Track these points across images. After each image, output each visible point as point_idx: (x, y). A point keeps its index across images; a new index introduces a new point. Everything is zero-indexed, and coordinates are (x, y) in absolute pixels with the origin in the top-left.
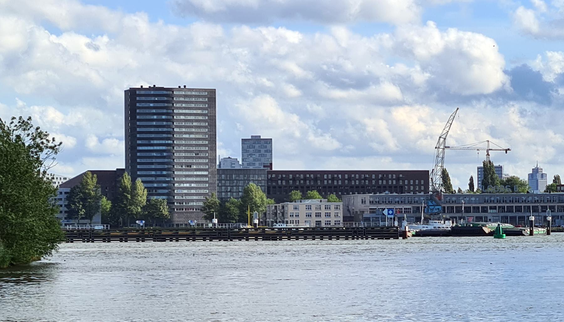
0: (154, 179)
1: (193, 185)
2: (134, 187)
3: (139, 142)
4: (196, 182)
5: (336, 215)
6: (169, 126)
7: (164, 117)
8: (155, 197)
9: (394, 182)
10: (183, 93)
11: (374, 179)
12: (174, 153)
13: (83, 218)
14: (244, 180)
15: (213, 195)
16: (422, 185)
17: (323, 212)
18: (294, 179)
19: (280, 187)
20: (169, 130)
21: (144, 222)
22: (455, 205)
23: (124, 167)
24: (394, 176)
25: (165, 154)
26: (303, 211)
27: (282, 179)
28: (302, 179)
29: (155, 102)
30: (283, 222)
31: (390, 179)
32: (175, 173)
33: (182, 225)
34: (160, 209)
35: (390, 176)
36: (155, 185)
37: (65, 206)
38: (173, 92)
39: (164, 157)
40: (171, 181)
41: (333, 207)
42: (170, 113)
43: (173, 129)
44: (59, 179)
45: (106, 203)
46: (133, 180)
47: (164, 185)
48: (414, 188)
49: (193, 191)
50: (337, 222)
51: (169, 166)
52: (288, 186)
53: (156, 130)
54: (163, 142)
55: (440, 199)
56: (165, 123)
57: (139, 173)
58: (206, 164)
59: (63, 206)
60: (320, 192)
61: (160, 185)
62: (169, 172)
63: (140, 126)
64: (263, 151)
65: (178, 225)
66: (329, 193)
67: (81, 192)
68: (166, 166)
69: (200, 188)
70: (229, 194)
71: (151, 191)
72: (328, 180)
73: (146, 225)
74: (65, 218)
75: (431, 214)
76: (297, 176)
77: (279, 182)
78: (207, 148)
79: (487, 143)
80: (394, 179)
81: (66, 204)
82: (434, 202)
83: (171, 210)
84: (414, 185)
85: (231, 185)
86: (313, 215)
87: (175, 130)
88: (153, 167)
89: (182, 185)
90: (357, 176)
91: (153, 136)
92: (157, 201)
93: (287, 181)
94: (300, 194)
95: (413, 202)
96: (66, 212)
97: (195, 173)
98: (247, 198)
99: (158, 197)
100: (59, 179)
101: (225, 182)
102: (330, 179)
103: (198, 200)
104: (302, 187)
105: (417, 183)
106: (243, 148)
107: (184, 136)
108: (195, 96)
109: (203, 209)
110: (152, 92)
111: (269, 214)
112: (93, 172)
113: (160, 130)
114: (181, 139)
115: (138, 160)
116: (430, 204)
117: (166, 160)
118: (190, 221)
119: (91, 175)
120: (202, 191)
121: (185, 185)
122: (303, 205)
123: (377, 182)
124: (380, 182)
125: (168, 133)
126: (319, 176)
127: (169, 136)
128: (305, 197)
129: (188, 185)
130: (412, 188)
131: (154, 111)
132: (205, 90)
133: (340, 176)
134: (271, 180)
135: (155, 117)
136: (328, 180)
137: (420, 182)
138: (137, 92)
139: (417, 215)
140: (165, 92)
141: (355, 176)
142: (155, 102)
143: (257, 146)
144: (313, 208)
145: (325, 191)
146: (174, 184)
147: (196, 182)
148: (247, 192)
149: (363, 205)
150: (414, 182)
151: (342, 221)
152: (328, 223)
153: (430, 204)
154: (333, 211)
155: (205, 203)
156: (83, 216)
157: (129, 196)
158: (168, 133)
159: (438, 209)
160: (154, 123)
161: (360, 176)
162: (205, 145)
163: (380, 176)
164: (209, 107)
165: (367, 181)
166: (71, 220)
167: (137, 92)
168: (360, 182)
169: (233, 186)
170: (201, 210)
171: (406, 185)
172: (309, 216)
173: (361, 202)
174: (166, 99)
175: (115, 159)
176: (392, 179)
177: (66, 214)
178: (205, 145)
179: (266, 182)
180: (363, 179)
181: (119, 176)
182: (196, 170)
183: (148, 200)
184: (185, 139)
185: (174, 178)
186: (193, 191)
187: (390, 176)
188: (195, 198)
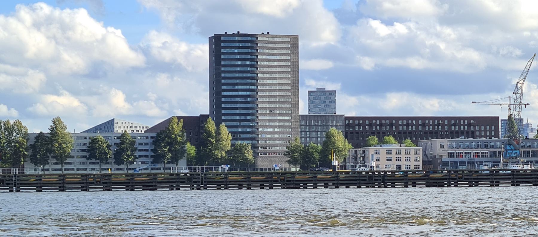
0: (238, 124)
1: (276, 130)
2: (218, 132)
3: (224, 87)
4: (279, 127)
5: (416, 160)
6: (253, 72)
7: (248, 63)
8: (240, 142)
9: (466, 127)
10: (267, 39)
11: (446, 125)
12: (257, 99)
13: (169, 163)
14: (324, 126)
15: (296, 139)
16: (493, 131)
17: (403, 156)
18: (370, 125)
19: (357, 133)
20: (253, 75)
21: (229, 166)
22: (531, 150)
23: (208, 114)
24: (466, 121)
25: (249, 99)
26: (382, 156)
27: (359, 125)
28: (378, 125)
29: (239, 48)
30: (364, 166)
31: (462, 125)
32: (259, 118)
33: (265, 169)
34: (245, 153)
35: (462, 122)
36: (240, 130)
37: (152, 150)
38: (257, 38)
39: (248, 102)
40: (254, 126)
41: (412, 152)
42: (254, 59)
43: (257, 74)
44: (141, 127)
45: (190, 149)
46: (218, 125)
47: (248, 130)
48: (490, 133)
49: (276, 136)
50: (417, 167)
51: (254, 111)
52: (362, 131)
53: (241, 75)
54: (248, 87)
55: (518, 144)
56: (249, 69)
57: (223, 118)
58: (289, 109)
59: (149, 150)
60: (394, 136)
61: (244, 130)
62: (254, 117)
63: (225, 72)
64: (327, 101)
65: (261, 169)
66: (404, 138)
67: (167, 136)
68: (250, 111)
69: (283, 133)
70: (308, 139)
71: (235, 136)
72: (403, 125)
73: (231, 169)
74: (152, 163)
75: (510, 159)
76: (374, 121)
77: (357, 127)
78: (290, 94)
79: (508, 99)
80: (466, 125)
81: (153, 148)
82: (512, 147)
83: (256, 155)
84: (485, 131)
85: (311, 130)
86: (394, 159)
87: (259, 75)
88: (238, 112)
89: (266, 130)
90: (431, 122)
91: (237, 81)
92: (242, 146)
93: (364, 127)
94: (376, 139)
95: (489, 147)
96: (152, 156)
97: (279, 118)
98: (328, 143)
99: (243, 142)
100: (141, 127)
101: (305, 128)
102: (405, 125)
103: (281, 145)
104: (379, 133)
105: (488, 129)
106: (309, 99)
107: (268, 82)
108: (279, 42)
109: (287, 154)
110: (237, 38)
111: (349, 158)
112: (179, 118)
113: (245, 75)
114: (265, 84)
115: (223, 106)
116: (508, 148)
117: (250, 105)
118: (274, 166)
119: (176, 121)
120: (284, 136)
121: (269, 130)
122: (383, 150)
123: (450, 128)
124: (453, 127)
125: (252, 78)
126: (394, 122)
127: (253, 81)
128: (382, 142)
129: (271, 130)
130: (488, 133)
131: (238, 57)
132: (288, 36)
133: (414, 122)
134: (349, 125)
135: (239, 63)
136: (403, 125)
137: (490, 128)
138: (222, 38)
139: (495, 159)
140: (249, 38)
141: (429, 122)
142: (239, 48)
143: (322, 97)
144: (394, 152)
145: (400, 137)
146: (258, 129)
147: (279, 127)
148: (329, 136)
149: (441, 150)
150: (485, 128)
151: (421, 165)
152: (409, 167)
153: (508, 148)
154: (412, 156)
155: (288, 148)
156: (170, 160)
157: (213, 141)
158: (252, 78)
159: (516, 153)
160: (239, 69)
161: (433, 122)
162: (288, 91)
163: (453, 122)
164: (292, 53)
165: (440, 127)
166: (157, 165)
167: (222, 38)
168: (433, 128)
169: (312, 132)
170: (284, 154)
171: (477, 131)
172: (390, 160)
173: (441, 147)
174: (250, 45)
175: (200, 104)
176: (464, 125)
177: (153, 158)
178: (288, 91)
179: (344, 127)
180: (436, 125)
181: (202, 122)
182: (280, 115)
183: (233, 145)
184: (269, 84)
185: (258, 123)
186: (276, 136)
187: (462, 122)
188: (278, 142)
